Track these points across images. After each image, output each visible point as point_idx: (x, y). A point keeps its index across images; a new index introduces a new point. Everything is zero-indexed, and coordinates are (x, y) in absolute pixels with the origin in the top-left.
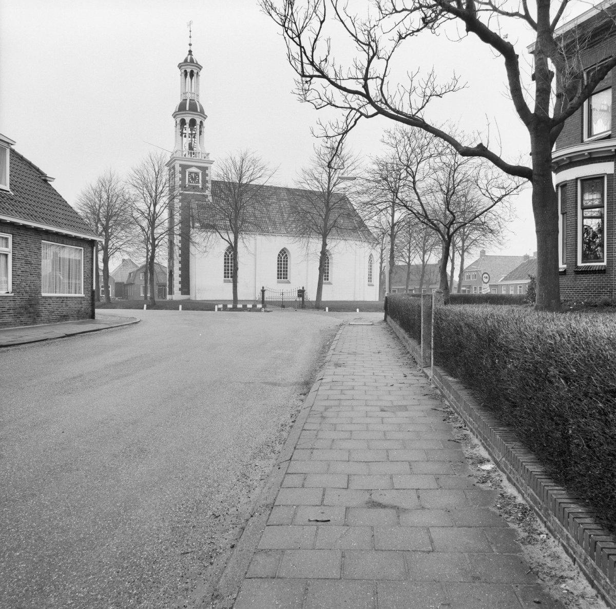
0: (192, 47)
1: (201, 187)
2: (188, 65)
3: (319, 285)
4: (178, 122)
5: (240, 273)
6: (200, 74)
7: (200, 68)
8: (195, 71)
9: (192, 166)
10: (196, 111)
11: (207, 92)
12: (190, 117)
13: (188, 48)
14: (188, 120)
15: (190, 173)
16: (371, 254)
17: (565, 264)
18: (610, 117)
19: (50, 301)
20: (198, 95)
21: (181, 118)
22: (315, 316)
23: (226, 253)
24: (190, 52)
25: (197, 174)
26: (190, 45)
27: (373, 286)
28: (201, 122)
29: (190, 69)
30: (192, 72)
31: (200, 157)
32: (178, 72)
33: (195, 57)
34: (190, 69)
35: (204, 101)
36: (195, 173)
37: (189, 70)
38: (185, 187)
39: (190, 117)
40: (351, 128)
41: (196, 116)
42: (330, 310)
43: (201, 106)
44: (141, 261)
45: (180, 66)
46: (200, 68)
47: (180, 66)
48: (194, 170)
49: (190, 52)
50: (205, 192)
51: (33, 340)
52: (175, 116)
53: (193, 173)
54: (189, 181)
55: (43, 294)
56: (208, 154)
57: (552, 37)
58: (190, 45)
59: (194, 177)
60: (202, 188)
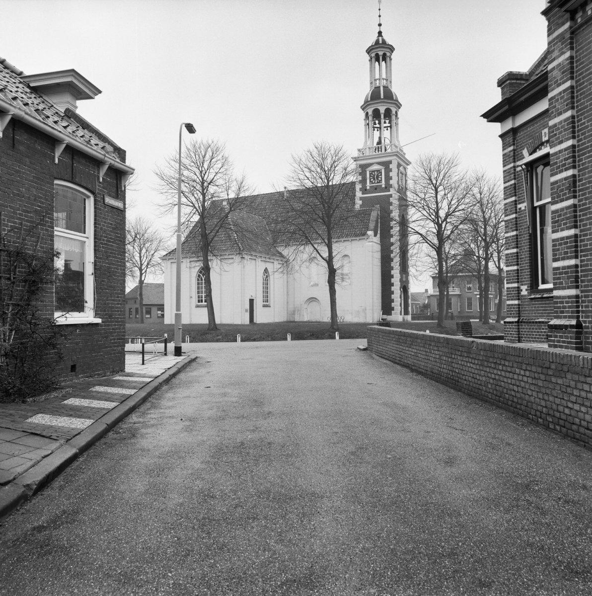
0: (381, 27)
1: (383, 186)
2: (379, 47)
3: (331, 305)
4: (370, 113)
7: (392, 49)
8: (381, 53)
12: (381, 107)
15: (372, 172)
16: (266, 268)
19: (434, 331)
20: (391, 82)
21: (373, 109)
23: (199, 276)
24: (380, 33)
25: (379, 171)
26: (380, 25)
28: (396, 112)
29: (380, 52)
30: (384, 55)
34: (380, 52)
36: (377, 171)
38: (366, 190)
39: (381, 107)
41: (377, 105)
42: (341, 338)
47: (369, 51)
48: (376, 167)
49: (380, 33)
50: (389, 191)
51: (104, 417)
52: (363, 108)
53: (375, 171)
54: (370, 181)
56: (359, 150)
58: (380, 25)
59: (376, 175)
60: (386, 187)
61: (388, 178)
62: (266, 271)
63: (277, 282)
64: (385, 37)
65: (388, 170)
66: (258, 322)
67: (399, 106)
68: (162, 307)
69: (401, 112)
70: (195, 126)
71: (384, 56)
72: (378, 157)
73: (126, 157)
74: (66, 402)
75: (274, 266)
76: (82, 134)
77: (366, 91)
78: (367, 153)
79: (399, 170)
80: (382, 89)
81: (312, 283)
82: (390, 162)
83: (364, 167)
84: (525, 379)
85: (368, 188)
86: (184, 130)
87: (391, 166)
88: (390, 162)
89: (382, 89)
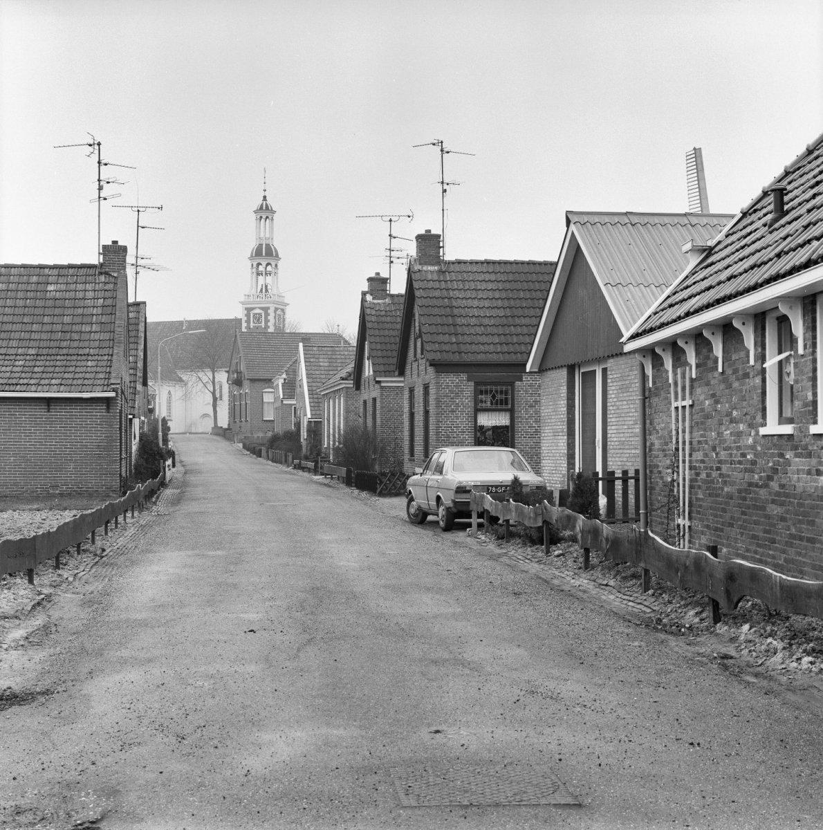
4: (255, 266)
6: (274, 218)
9: (253, 309)
10: (272, 255)
12: (265, 254)
14: (264, 217)
15: (255, 314)
17: (790, 421)
18: (776, 334)
24: (265, 197)
25: (260, 314)
26: (265, 191)
27: (697, 153)
29: (265, 211)
31: (276, 299)
32: (254, 216)
33: (269, 201)
34: (265, 211)
35: (277, 244)
37: (259, 217)
39: (265, 254)
43: (276, 251)
45: (255, 212)
47: (255, 212)
48: (258, 311)
49: (265, 197)
52: (251, 258)
57: (783, 209)
58: (265, 191)
61: (267, 321)
62: (169, 393)
65: (267, 315)
69: (280, 264)
70: (115, 240)
71: (267, 217)
72: (602, 258)
74: (68, 516)
77: (252, 245)
78: (251, 299)
79: (276, 314)
80: (264, 246)
81: (206, 403)
82: (269, 308)
83: (249, 310)
85: (252, 327)
86: (411, 214)
87: (269, 311)
88: (269, 308)
89: (264, 246)
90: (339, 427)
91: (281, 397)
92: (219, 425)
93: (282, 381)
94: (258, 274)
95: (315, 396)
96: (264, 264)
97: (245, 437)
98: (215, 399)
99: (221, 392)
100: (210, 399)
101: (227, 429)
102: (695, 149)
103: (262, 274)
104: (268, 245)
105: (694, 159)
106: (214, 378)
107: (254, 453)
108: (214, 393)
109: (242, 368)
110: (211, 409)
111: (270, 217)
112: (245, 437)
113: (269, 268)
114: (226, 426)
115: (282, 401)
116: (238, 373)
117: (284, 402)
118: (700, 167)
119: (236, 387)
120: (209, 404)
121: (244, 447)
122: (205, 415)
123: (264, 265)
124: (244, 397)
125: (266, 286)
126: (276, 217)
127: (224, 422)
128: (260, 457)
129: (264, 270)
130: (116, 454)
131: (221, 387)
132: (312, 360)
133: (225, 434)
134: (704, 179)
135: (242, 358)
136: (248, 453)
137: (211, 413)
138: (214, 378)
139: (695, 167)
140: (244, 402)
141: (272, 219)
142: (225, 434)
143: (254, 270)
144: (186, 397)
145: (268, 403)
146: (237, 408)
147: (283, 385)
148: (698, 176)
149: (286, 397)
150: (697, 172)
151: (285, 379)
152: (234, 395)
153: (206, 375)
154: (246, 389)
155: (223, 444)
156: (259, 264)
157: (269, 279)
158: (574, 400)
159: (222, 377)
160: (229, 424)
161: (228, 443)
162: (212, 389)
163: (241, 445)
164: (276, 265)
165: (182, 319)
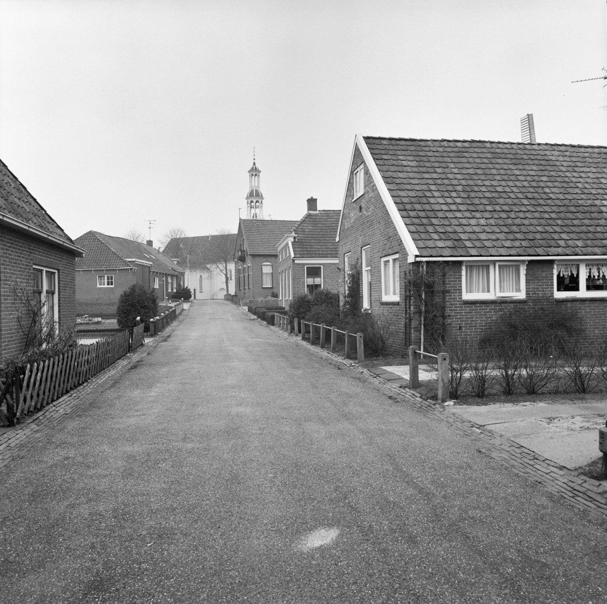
4: (249, 202)
5: (482, 139)
7: (260, 172)
10: (259, 196)
11: (255, 161)
12: (255, 197)
13: (253, 161)
14: (254, 174)
22: (345, 384)
24: (254, 163)
26: (254, 159)
27: (530, 118)
28: (261, 202)
29: (254, 172)
32: (248, 174)
34: (254, 172)
35: (262, 190)
37: (251, 174)
39: (255, 197)
40: (353, 173)
43: (261, 194)
44: (590, 382)
46: (260, 172)
47: (249, 172)
49: (254, 163)
55: (466, 296)
58: (254, 159)
62: (201, 276)
63: (206, 283)
64: (256, 166)
66: (237, 233)
67: (262, 198)
68: (486, 290)
69: (264, 201)
71: (256, 175)
73: (79, 236)
75: (205, 275)
76: (361, 371)
77: (247, 191)
84: (557, 229)
90: (507, 275)
91: (293, 255)
92: (229, 293)
93: (292, 239)
94: (251, 207)
95: (412, 214)
96: (255, 201)
97: (250, 301)
98: (227, 279)
99: (231, 274)
100: (224, 280)
101: (234, 296)
102: (528, 115)
103: (253, 207)
104: (256, 190)
105: (528, 124)
106: (226, 266)
107: (264, 319)
108: (226, 275)
109: (246, 247)
110: (225, 284)
111: (258, 174)
112: (250, 301)
113: (257, 204)
114: (233, 294)
115: (294, 260)
116: (242, 251)
117: (296, 262)
118: (531, 126)
119: (240, 263)
120: (224, 282)
121: (250, 310)
122: (222, 289)
123: (255, 202)
124: (247, 270)
125: (256, 215)
126: (261, 174)
127: (232, 291)
128: (273, 324)
129: (254, 204)
130: (6, 330)
131: (231, 272)
132: (385, 157)
133: (233, 299)
134: (534, 134)
135: (245, 241)
136: (255, 317)
137: (225, 288)
138: (226, 266)
139: (528, 126)
140: (247, 274)
141: (259, 176)
142: (233, 299)
143: (249, 205)
144: (210, 277)
145: (266, 274)
146: (242, 279)
147: (293, 243)
148: (530, 132)
149: (298, 256)
150: (530, 130)
151: (295, 238)
152: (239, 269)
153: (222, 266)
154: (249, 263)
155: (231, 307)
156: (252, 202)
157: (258, 211)
158: (485, 285)
159: (232, 266)
160: (235, 293)
161: (234, 306)
162: (225, 272)
163: (246, 308)
164: (261, 202)
165: (208, 235)
